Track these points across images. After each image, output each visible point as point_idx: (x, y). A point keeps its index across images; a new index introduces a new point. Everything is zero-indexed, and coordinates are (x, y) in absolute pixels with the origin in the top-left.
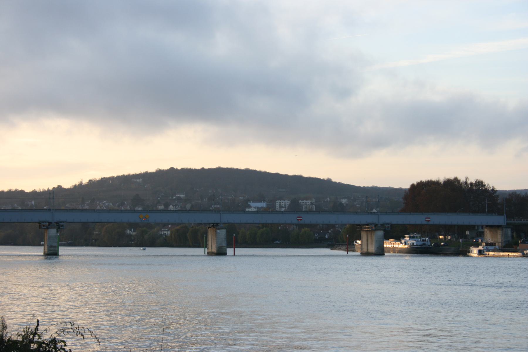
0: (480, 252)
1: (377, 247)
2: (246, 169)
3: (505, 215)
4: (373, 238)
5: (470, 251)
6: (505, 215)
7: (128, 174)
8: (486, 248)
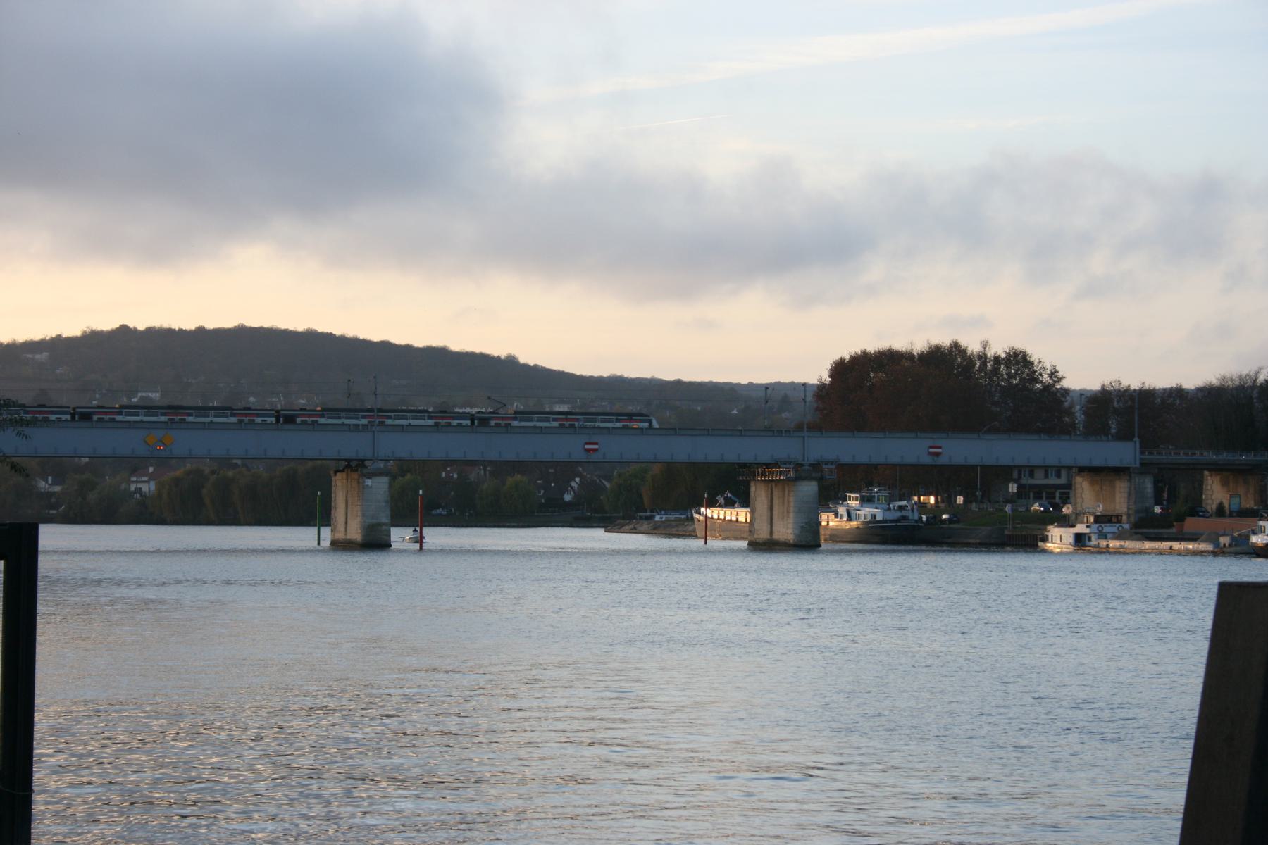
0: (1080, 539)
1: (802, 527)
2: (307, 330)
3: (1136, 439)
4: (789, 502)
5: (1047, 536)
6: (1136, 439)
7: (11, 342)
8: (1098, 528)
